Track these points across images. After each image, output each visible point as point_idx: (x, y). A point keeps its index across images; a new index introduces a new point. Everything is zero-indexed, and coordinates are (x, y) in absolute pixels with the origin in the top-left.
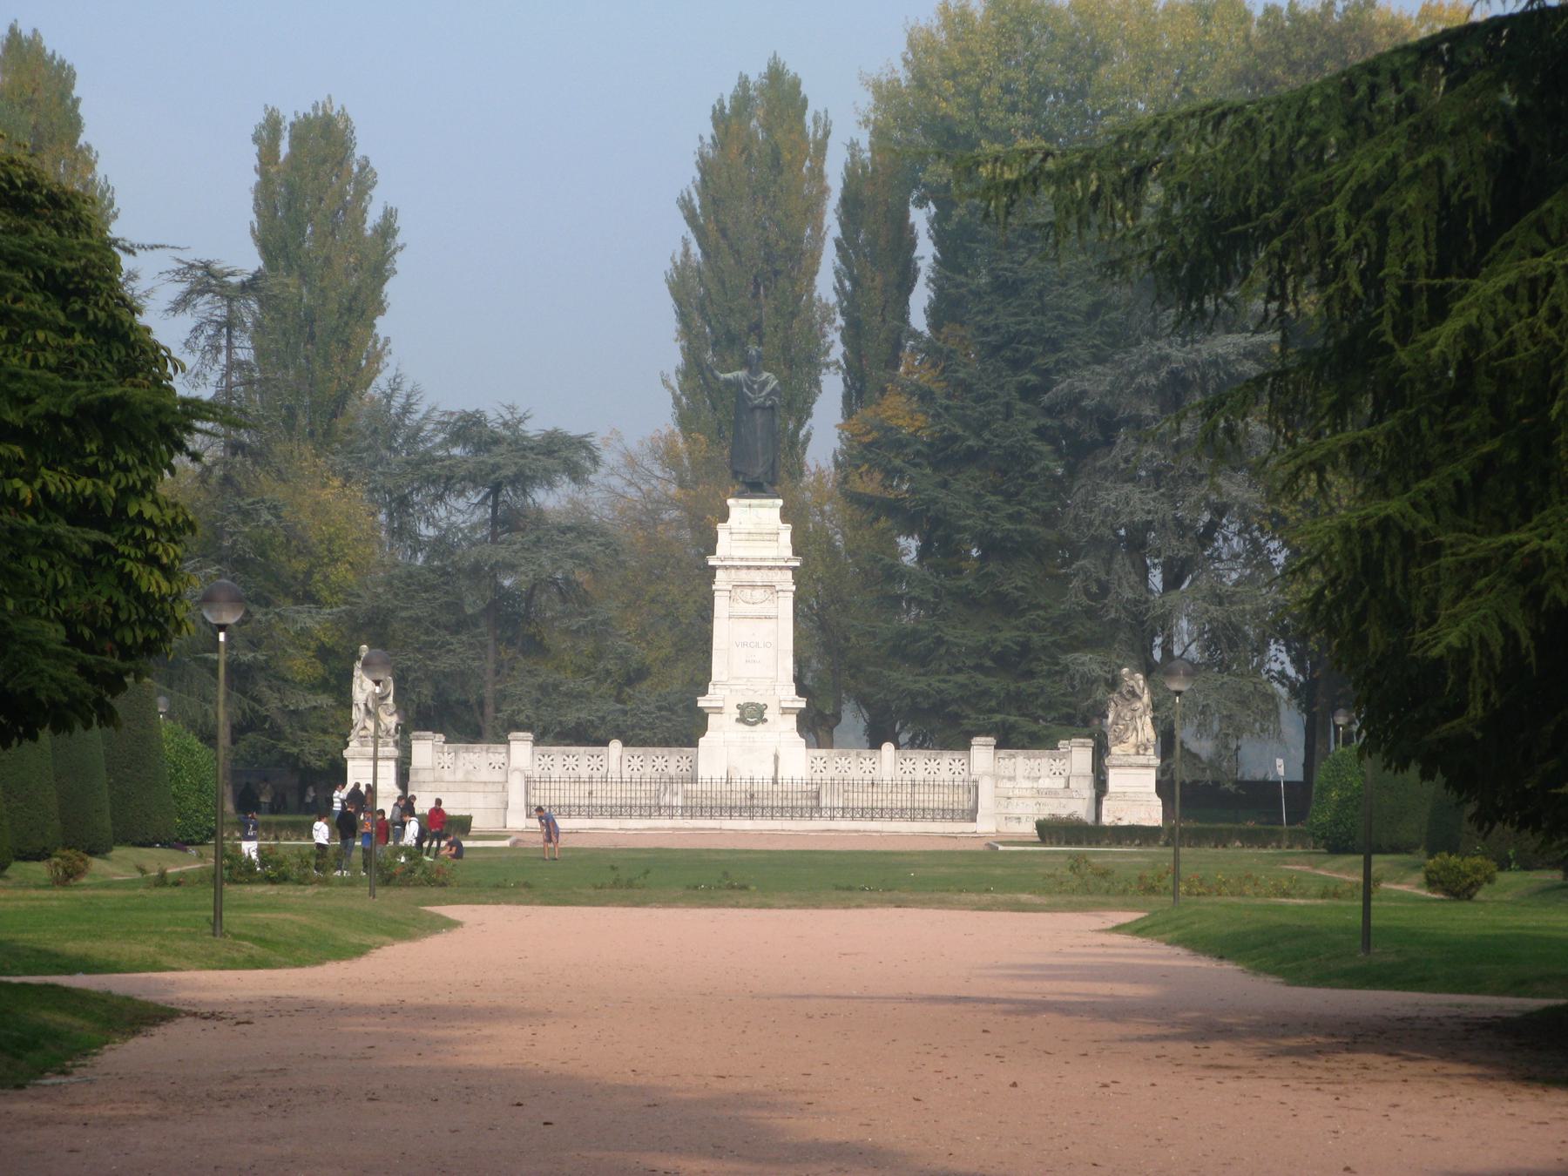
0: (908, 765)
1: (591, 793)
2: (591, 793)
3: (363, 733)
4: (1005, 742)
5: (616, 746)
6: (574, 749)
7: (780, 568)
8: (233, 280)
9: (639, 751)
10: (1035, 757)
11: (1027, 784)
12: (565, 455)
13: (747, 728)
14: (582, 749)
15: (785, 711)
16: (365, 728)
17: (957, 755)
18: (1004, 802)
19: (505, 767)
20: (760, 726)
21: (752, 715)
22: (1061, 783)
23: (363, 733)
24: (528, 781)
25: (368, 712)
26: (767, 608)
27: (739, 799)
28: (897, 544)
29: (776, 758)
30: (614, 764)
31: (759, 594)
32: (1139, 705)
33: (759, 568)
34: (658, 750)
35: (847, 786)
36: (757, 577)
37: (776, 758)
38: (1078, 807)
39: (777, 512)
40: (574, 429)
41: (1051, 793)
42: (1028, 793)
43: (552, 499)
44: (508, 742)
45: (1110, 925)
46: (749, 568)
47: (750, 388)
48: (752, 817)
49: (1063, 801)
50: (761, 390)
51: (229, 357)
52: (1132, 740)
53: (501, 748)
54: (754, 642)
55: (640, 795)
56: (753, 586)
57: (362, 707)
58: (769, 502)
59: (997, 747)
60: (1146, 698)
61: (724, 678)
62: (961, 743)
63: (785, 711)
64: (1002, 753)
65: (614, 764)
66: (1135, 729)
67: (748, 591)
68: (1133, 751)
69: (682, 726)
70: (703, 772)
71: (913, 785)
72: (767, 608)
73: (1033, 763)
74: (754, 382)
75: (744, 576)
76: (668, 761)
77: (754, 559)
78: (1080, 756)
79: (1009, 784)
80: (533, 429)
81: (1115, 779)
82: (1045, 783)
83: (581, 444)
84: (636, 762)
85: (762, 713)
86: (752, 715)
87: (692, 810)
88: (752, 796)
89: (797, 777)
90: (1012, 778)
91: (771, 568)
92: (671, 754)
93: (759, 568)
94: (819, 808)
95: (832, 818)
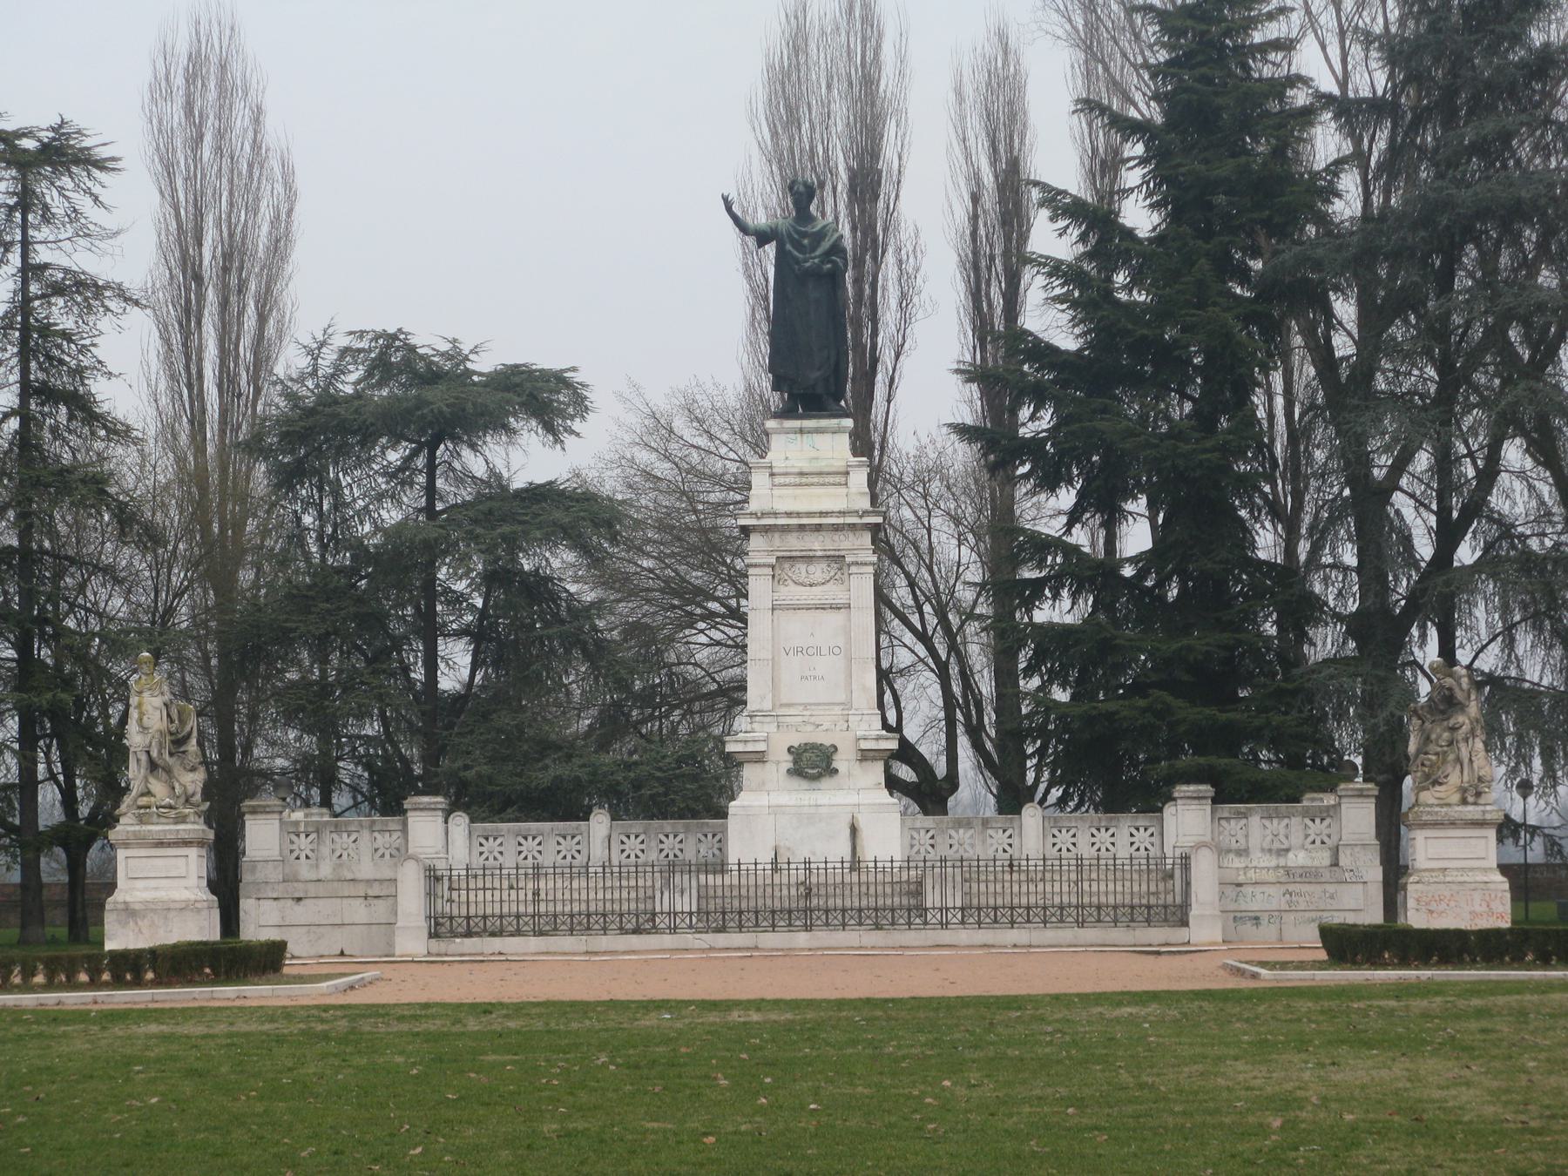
0: (1064, 838)
1: (536, 893)
2: (536, 893)
3: (143, 801)
4: (1234, 791)
5: (600, 822)
6: (534, 826)
7: (853, 527)
8: (28, 144)
9: (637, 826)
10: (1281, 817)
11: (1272, 861)
12: (542, 397)
13: (804, 784)
14: (546, 826)
15: (865, 756)
16: (148, 793)
17: (1142, 820)
18: (1230, 891)
19: (401, 854)
20: (826, 783)
21: (813, 763)
22: (1324, 858)
23: (143, 801)
24: (433, 876)
25: (153, 766)
26: (833, 593)
27: (788, 896)
28: (1165, 113)
29: (854, 830)
30: (598, 852)
31: (818, 571)
32: (1461, 719)
33: (818, 528)
34: (668, 825)
35: (971, 870)
36: (816, 543)
37: (854, 830)
38: (1361, 905)
39: (845, 440)
40: (545, 359)
41: (1309, 875)
42: (1271, 877)
43: (526, 459)
44: (403, 812)
45: (929, 943)
46: (802, 528)
47: (798, 246)
48: (808, 928)
49: (1331, 888)
50: (813, 249)
51: (25, 256)
52: (1454, 779)
53: (393, 822)
54: (811, 663)
55: (624, 899)
56: (809, 559)
57: (144, 758)
58: (833, 422)
59: (1215, 801)
60: (1473, 709)
61: (767, 705)
62: (1142, 796)
63: (865, 756)
64: (1226, 809)
65: (598, 852)
66: (1459, 760)
67: (802, 567)
68: (1456, 798)
69: (694, 789)
70: (736, 851)
71: (1079, 867)
72: (833, 593)
73: (1277, 826)
74: (804, 235)
75: (795, 543)
76: (678, 840)
77: (810, 514)
78: (1358, 817)
79: (1238, 863)
80: (483, 365)
81: (1423, 849)
82: (1298, 858)
83: (558, 380)
84: (633, 844)
85: (829, 763)
86: (813, 763)
87: (718, 916)
88: (808, 895)
89: (883, 856)
90: (1243, 852)
91: (836, 528)
92: (687, 830)
93: (818, 528)
94: (922, 910)
95: (944, 925)
